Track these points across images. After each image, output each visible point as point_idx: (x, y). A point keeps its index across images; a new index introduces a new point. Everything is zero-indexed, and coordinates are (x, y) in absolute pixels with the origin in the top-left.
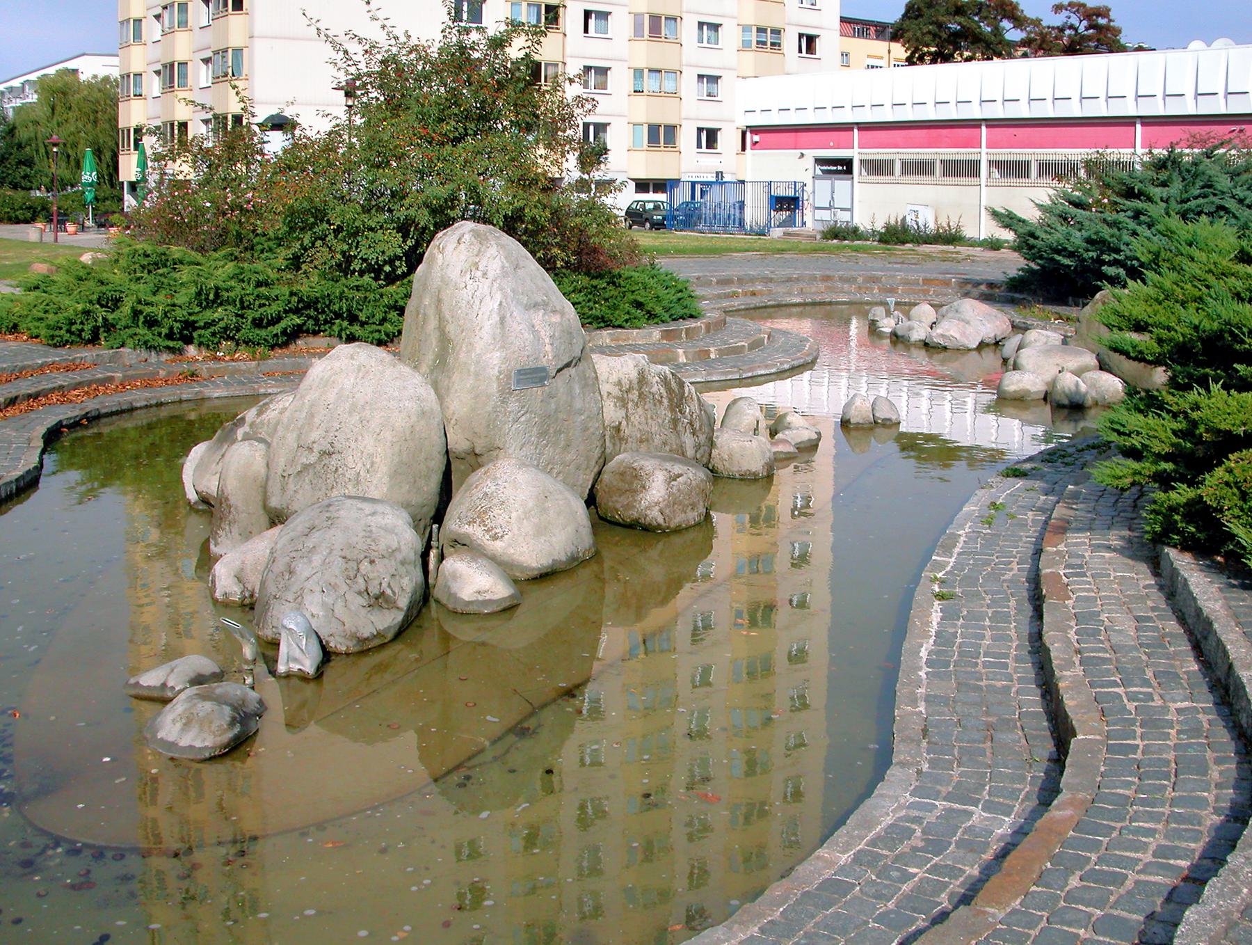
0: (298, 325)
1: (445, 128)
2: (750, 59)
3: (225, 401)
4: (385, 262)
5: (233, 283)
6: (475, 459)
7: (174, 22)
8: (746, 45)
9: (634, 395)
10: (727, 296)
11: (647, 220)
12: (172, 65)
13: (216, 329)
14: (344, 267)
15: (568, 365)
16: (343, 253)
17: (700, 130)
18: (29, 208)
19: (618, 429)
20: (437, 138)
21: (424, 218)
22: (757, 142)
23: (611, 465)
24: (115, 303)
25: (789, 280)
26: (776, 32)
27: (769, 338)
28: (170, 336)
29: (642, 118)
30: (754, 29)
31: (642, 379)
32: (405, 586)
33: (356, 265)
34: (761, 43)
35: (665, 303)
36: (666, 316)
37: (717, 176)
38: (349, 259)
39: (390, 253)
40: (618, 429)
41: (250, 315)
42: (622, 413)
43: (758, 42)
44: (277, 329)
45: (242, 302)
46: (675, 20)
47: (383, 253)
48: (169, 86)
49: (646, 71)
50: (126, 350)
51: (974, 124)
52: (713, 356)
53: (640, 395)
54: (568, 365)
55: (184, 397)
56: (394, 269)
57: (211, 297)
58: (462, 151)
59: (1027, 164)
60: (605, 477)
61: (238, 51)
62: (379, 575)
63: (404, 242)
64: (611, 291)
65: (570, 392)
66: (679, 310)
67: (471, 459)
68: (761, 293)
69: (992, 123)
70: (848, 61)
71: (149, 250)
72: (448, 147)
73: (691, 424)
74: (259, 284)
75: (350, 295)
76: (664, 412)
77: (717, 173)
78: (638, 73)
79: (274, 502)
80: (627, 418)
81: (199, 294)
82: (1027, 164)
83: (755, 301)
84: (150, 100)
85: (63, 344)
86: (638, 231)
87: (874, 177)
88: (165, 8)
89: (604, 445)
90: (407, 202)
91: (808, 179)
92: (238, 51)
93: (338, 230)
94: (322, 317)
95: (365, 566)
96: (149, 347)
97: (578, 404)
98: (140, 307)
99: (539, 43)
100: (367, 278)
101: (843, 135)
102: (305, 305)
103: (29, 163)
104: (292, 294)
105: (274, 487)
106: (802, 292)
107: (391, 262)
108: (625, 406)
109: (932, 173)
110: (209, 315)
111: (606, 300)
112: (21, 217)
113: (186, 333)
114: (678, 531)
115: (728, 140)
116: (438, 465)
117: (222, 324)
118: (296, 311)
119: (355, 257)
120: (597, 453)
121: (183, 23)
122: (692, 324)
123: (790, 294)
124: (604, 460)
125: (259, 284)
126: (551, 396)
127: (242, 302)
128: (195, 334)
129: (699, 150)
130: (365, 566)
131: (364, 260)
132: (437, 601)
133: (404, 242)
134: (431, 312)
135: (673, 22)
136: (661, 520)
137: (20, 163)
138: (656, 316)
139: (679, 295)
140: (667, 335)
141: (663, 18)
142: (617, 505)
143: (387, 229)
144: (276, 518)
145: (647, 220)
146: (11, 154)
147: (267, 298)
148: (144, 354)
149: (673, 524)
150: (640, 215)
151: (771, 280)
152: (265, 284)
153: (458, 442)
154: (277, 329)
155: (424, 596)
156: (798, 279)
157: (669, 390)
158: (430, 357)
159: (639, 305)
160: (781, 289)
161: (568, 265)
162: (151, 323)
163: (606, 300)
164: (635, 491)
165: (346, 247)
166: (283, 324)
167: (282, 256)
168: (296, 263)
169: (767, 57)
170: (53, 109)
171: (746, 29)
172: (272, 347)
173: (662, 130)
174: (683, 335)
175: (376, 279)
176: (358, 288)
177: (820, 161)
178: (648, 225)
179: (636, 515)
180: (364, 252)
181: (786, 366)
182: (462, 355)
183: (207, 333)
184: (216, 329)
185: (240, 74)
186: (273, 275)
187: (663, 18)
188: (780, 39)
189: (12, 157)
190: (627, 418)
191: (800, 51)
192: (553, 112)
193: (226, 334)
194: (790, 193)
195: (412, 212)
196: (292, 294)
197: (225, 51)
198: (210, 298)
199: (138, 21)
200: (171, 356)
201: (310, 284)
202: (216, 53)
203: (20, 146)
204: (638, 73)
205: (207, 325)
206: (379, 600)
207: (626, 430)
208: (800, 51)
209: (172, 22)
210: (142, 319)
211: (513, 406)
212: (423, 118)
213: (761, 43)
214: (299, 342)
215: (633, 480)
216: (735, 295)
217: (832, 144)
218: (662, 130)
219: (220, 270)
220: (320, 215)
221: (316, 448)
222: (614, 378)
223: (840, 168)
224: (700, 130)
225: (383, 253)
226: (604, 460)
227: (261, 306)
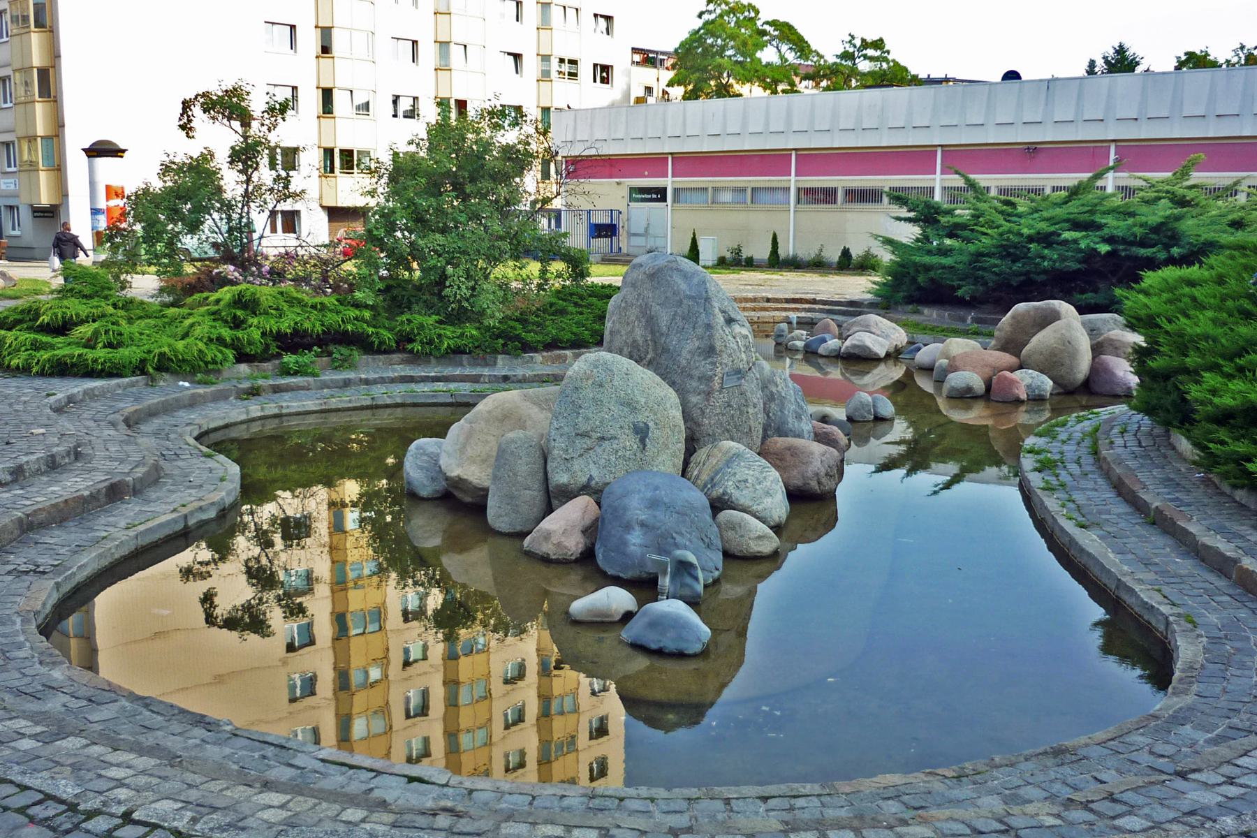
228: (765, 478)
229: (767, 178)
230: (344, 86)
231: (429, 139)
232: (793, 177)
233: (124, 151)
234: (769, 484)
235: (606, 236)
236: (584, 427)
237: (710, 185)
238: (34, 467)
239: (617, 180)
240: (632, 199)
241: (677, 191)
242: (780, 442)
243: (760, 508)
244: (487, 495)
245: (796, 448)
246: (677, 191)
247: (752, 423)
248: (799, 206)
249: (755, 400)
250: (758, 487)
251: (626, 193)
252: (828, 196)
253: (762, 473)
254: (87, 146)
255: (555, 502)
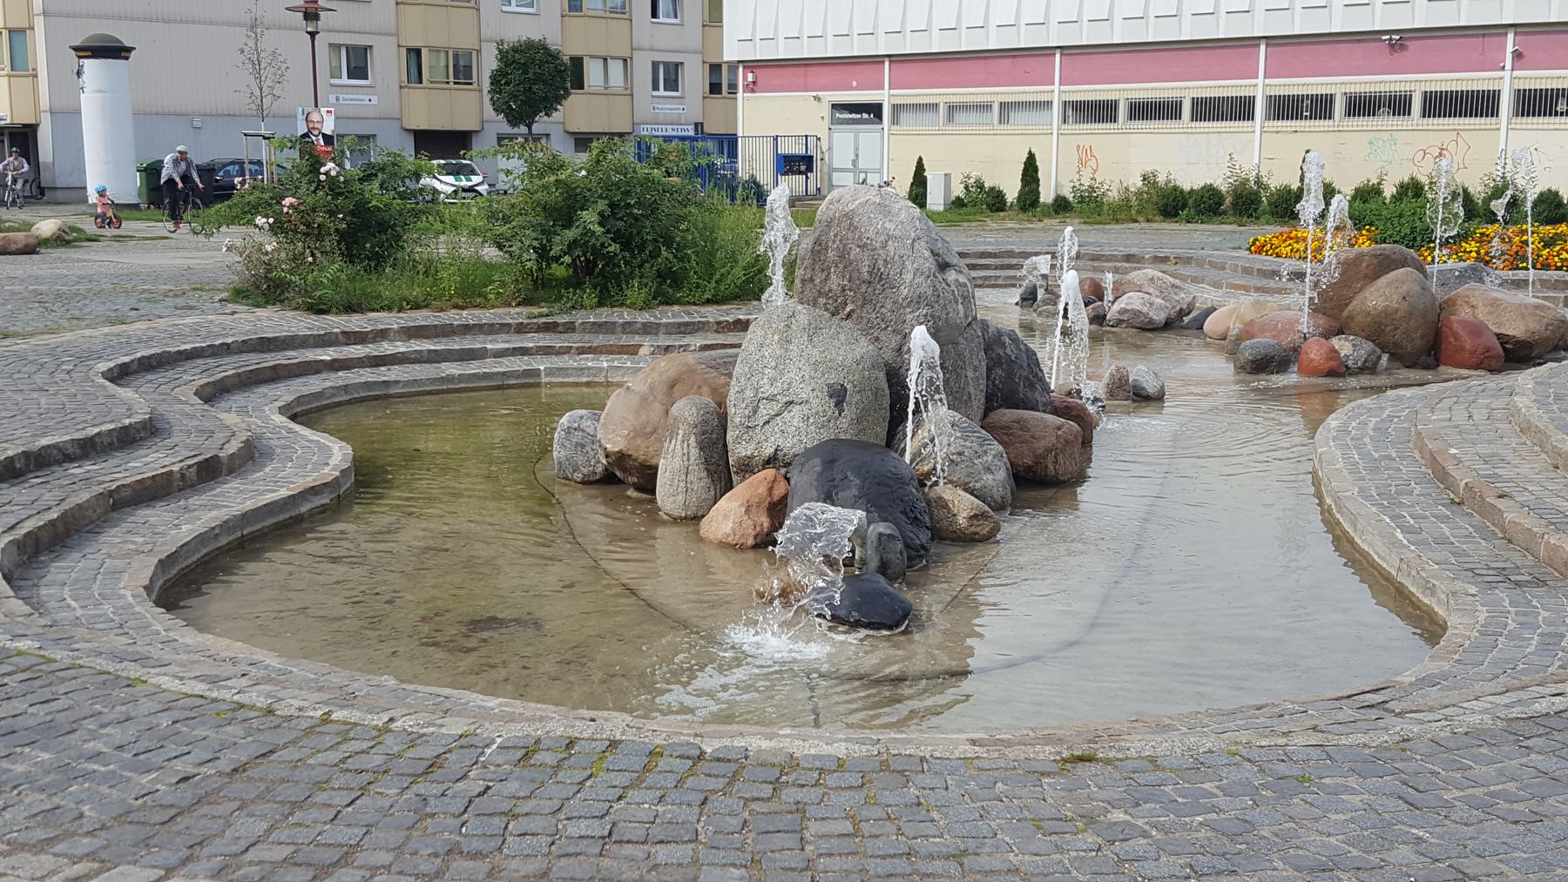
17: (655, 65)
27: (1337, 469)
37: (696, 130)
51: (876, 60)
59: (1426, 113)
69: (895, 59)
77: (696, 124)
82: (1426, 113)
101: (868, 71)
109: (1114, 119)
129: (655, 93)
143: (641, 266)
177: (837, 107)
182: (659, 741)
194: (799, 150)
217: (854, 83)
223: (865, 116)
228: (986, 452)
229: (1027, 88)
230: (559, 26)
231: (1377, 345)
232: (1056, 87)
233: (129, 50)
234: (990, 458)
235: (800, 173)
236: (767, 390)
237: (997, 100)
238: (106, 440)
239: (814, 94)
240: (834, 121)
241: (896, 109)
242: (1006, 415)
243: (978, 485)
244: (655, 474)
245: (1026, 421)
246: (896, 109)
247: (972, 390)
248: (1066, 126)
249: (976, 363)
250: (976, 461)
251: (826, 110)
252: (1320, 107)
253: (981, 445)
254: (77, 43)
255: (735, 478)
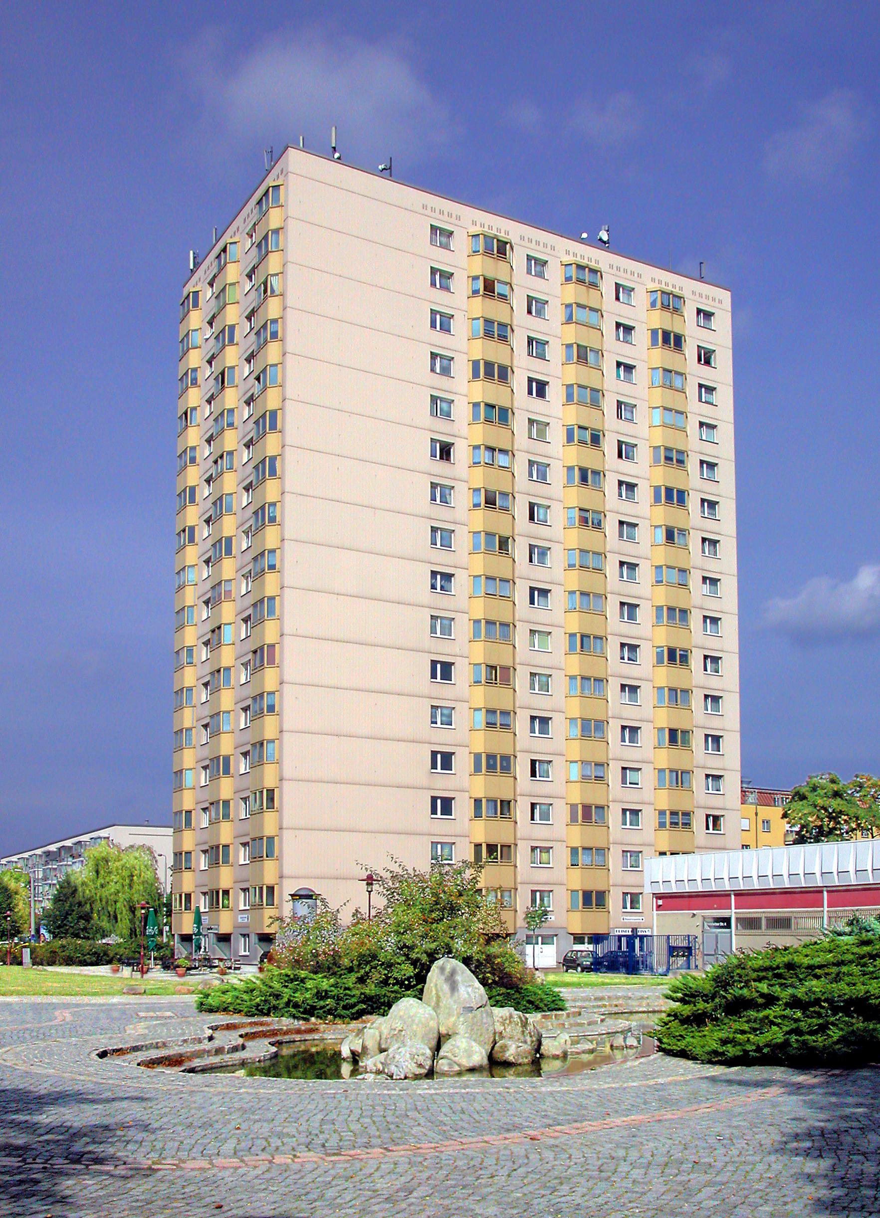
0: (364, 1009)
1: (434, 915)
2: (664, 839)
3: (333, 1041)
4: (405, 979)
5: (333, 988)
6: (448, 1036)
7: (219, 815)
8: (662, 825)
9: (508, 1022)
10: (599, 1006)
11: (579, 965)
12: (218, 847)
13: (326, 1009)
14: (385, 982)
15: (481, 1007)
16: (385, 975)
18: (95, 953)
19: (501, 1033)
20: (430, 920)
21: (424, 958)
22: (660, 906)
23: (498, 1045)
24: (278, 996)
25: (642, 998)
26: (687, 814)
28: (303, 1013)
29: (577, 886)
30: (668, 813)
31: (511, 1016)
32: (428, 1064)
33: (391, 981)
34: (674, 824)
35: (545, 1002)
36: (546, 1009)
38: (388, 978)
39: (407, 975)
40: (501, 1033)
41: (342, 1003)
42: (502, 1028)
43: (671, 823)
44: (354, 1011)
45: (338, 997)
46: (603, 808)
47: (405, 975)
48: (214, 863)
49: (580, 849)
50: (284, 1018)
52: (566, 1026)
53: (510, 1022)
54: (481, 1007)
55: (316, 1037)
56: (410, 982)
57: (323, 994)
58: (441, 927)
60: (496, 1048)
61: (271, 839)
62: (421, 1059)
63: (415, 970)
64: (517, 995)
65: (482, 1016)
66: (552, 1006)
67: (448, 1037)
68: (621, 1005)
70: (769, 828)
71: (289, 973)
72: (435, 925)
73: (530, 1033)
74: (346, 989)
75: (388, 994)
76: (519, 1029)
78: (574, 851)
79: (383, 1046)
80: (505, 1029)
81: (318, 992)
82: (768, 927)
83: (616, 1010)
84: (197, 871)
85: (253, 1015)
86: (572, 973)
87: (747, 931)
88: (212, 804)
89: (495, 1037)
90: (416, 950)
91: (698, 932)
92: (271, 839)
93: (383, 964)
94: (375, 1006)
95: (416, 1057)
96: (294, 1017)
97: (485, 1021)
98: (292, 999)
99: (480, 872)
100: (396, 987)
102: (367, 999)
103: (87, 918)
104: (362, 994)
105: (383, 1041)
106: (648, 1005)
107: (408, 979)
108: (504, 1025)
110: (322, 1003)
111: (514, 1000)
112: (89, 961)
113: (310, 1011)
114: (520, 1065)
115: (647, 903)
116: (436, 1035)
117: (328, 1007)
118: (363, 1002)
119: (391, 977)
120: (492, 1039)
121: (226, 816)
122: (560, 1012)
123: (640, 1006)
124: (495, 1043)
125: (346, 989)
126: (475, 1017)
127: (338, 997)
128: (316, 1012)
130: (416, 1057)
131: (395, 979)
132: (437, 1073)
133: (415, 970)
134: (434, 989)
135: (601, 809)
136: (514, 1061)
137: (81, 917)
138: (540, 1008)
139: (554, 998)
140: (544, 1017)
141: (593, 807)
142: (499, 1056)
144: (382, 1051)
145: (579, 965)
146: (73, 911)
147: (350, 995)
148: (292, 1020)
149: (518, 1062)
150: (574, 961)
151: (630, 998)
152: (348, 989)
153: (443, 1030)
154: (354, 1011)
155: (432, 1067)
156: (647, 998)
157: (521, 1021)
158: (433, 1004)
159: (530, 1002)
160: (635, 1003)
161: (494, 982)
162: (296, 1006)
163: (514, 1000)
164: (505, 1051)
165: (386, 972)
166: (356, 1008)
167: (353, 977)
168: (362, 980)
169: (680, 837)
170: (97, 872)
171: (662, 813)
172: (352, 1019)
173: (594, 894)
174: (553, 1017)
175: (401, 988)
176: (392, 992)
178: (579, 969)
179: (504, 1058)
180: (396, 975)
181: (604, 1032)
183: (321, 1011)
184: (326, 1009)
185: (273, 856)
186: (351, 986)
187: (593, 807)
188: (689, 820)
189: (75, 913)
190: (505, 1029)
191: (708, 828)
192: (486, 906)
193: (330, 1012)
195: (419, 955)
196: (362, 994)
197: (261, 838)
198: (321, 995)
199: (189, 812)
200: (304, 1022)
201: (371, 989)
202: (254, 840)
203: (80, 904)
204: (574, 851)
205: (322, 1008)
206: (420, 1066)
207: (504, 1034)
208: (708, 828)
209: (217, 813)
210: (292, 1003)
211: (461, 1019)
212: (423, 911)
213: (674, 824)
214: (364, 1017)
215: (504, 1048)
216: (605, 1006)
218: (594, 894)
219: (325, 984)
220: (374, 957)
221: (397, 1029)
222: (500, 1015)
223: (722, 924)
224: (625, 894)
225: (405, 975)
226: (495, 1043)
227: (347, 999)
